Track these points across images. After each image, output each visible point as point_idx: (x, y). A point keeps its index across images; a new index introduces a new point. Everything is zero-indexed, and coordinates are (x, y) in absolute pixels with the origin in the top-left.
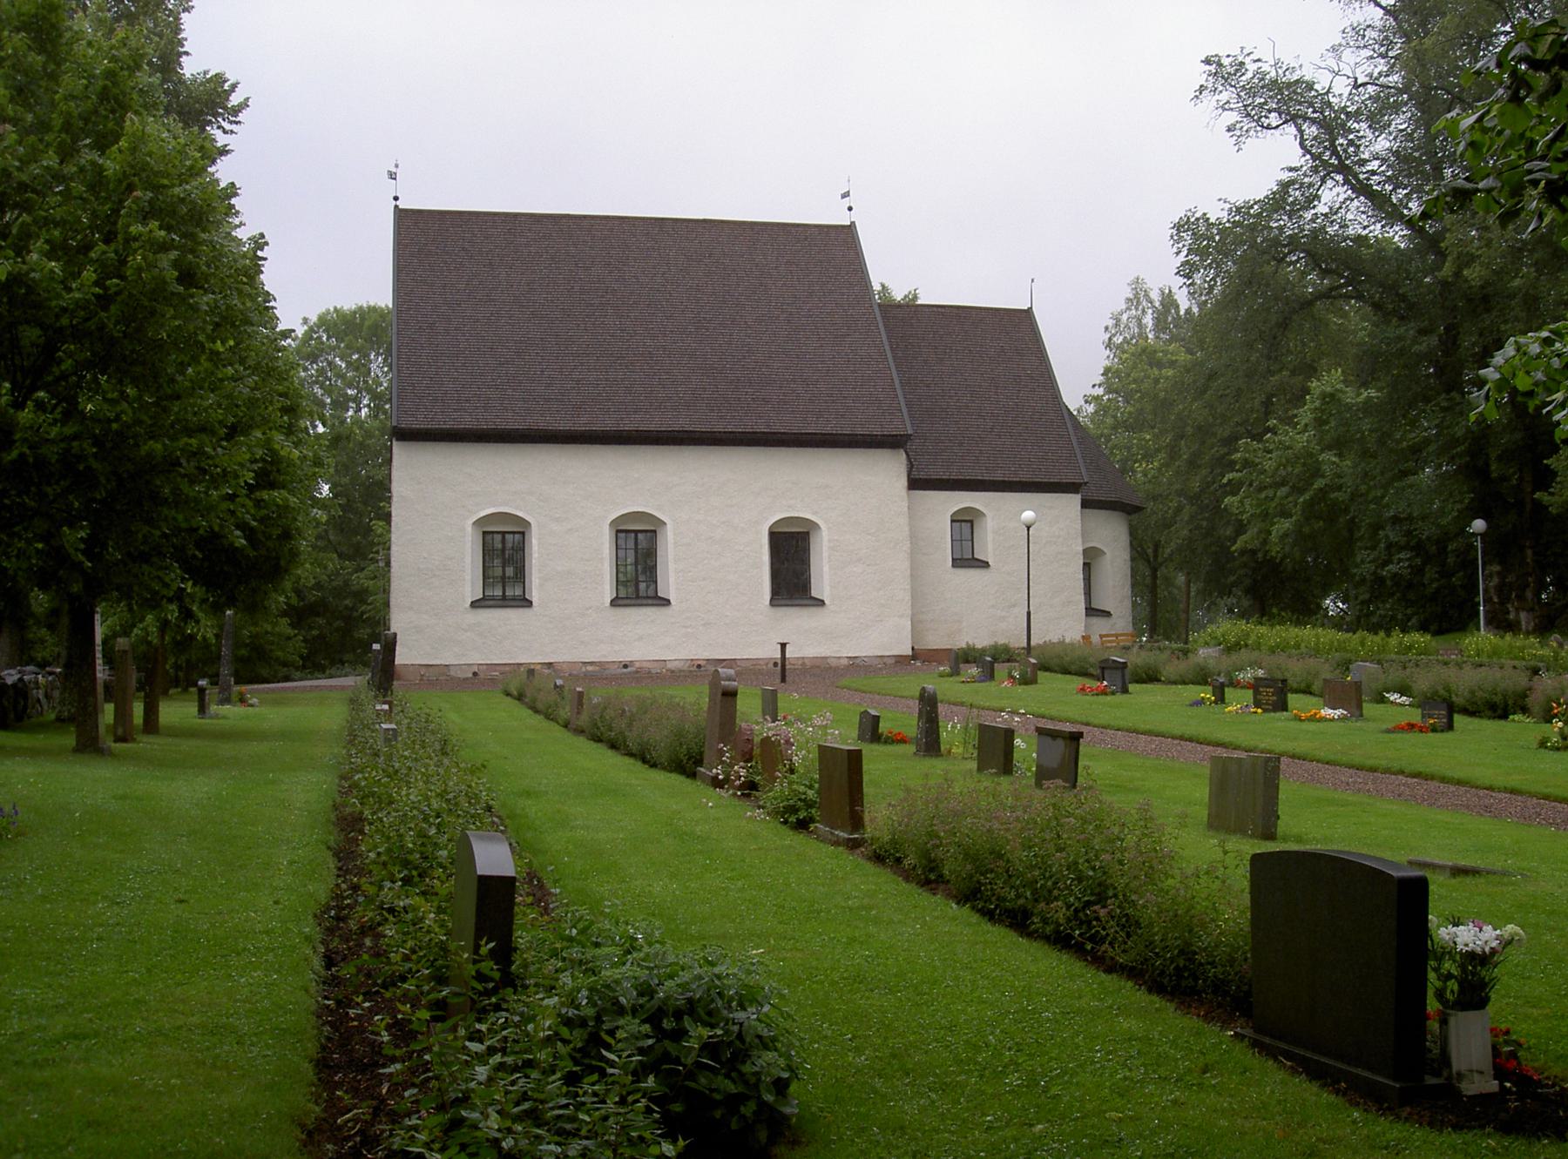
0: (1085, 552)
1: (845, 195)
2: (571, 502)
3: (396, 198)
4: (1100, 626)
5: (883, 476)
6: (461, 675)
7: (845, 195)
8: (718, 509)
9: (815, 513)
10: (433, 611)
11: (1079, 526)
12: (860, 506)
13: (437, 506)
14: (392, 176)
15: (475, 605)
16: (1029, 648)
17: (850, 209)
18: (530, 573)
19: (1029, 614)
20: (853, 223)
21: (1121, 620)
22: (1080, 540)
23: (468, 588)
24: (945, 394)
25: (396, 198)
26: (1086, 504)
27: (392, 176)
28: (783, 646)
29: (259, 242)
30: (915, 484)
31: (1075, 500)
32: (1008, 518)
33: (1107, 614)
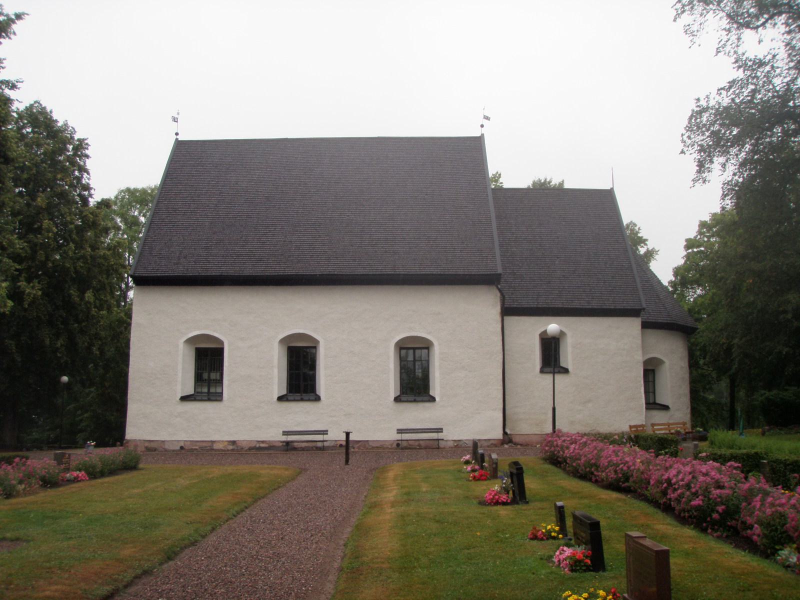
0: (646, 363)
1: (487, 118)
2: (254, 328)
3: (177, 134)
4: (659, 417)
5: (479, 309)
6: (172, 448)
7: (487, 118)
8: (359, 334)
9: (429, 333)
10: (157, 406)
11: (639, 342)
12: (463, 329)
13: (160, 330)
14: (175, 120)
15: (280, 399)
16: (507, 439)
17: (482, 126)
18: (202, 378)
19: (554, 409)
20: (482, 136)
21: (678, 413)
22: (640, 352)
23: (276, 387)
24: (551, 254)
25: (177, 134)
26: (645, 325)
27: (175, 120)
28: (348, 434)
29: (683, 258)
30: (507, 311)
31: (633, 325)
32: (580, 337)
33: (666, 408)
